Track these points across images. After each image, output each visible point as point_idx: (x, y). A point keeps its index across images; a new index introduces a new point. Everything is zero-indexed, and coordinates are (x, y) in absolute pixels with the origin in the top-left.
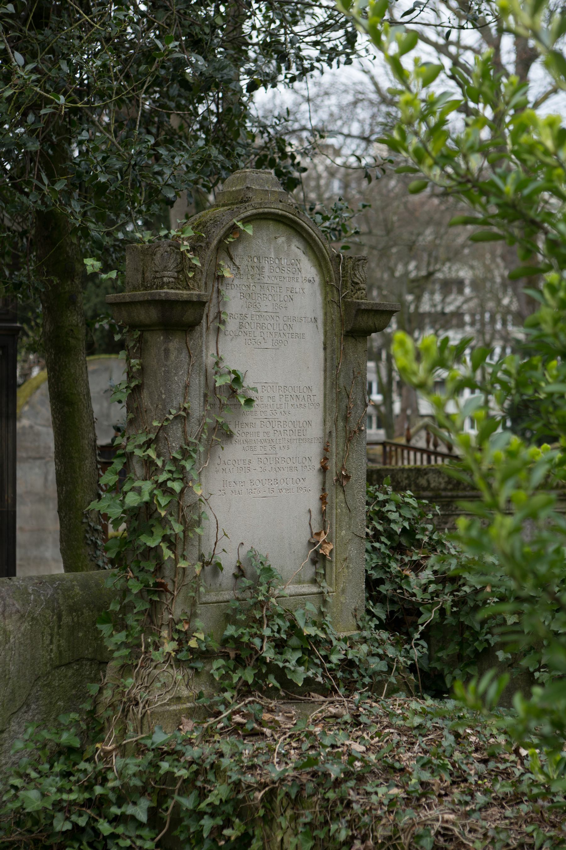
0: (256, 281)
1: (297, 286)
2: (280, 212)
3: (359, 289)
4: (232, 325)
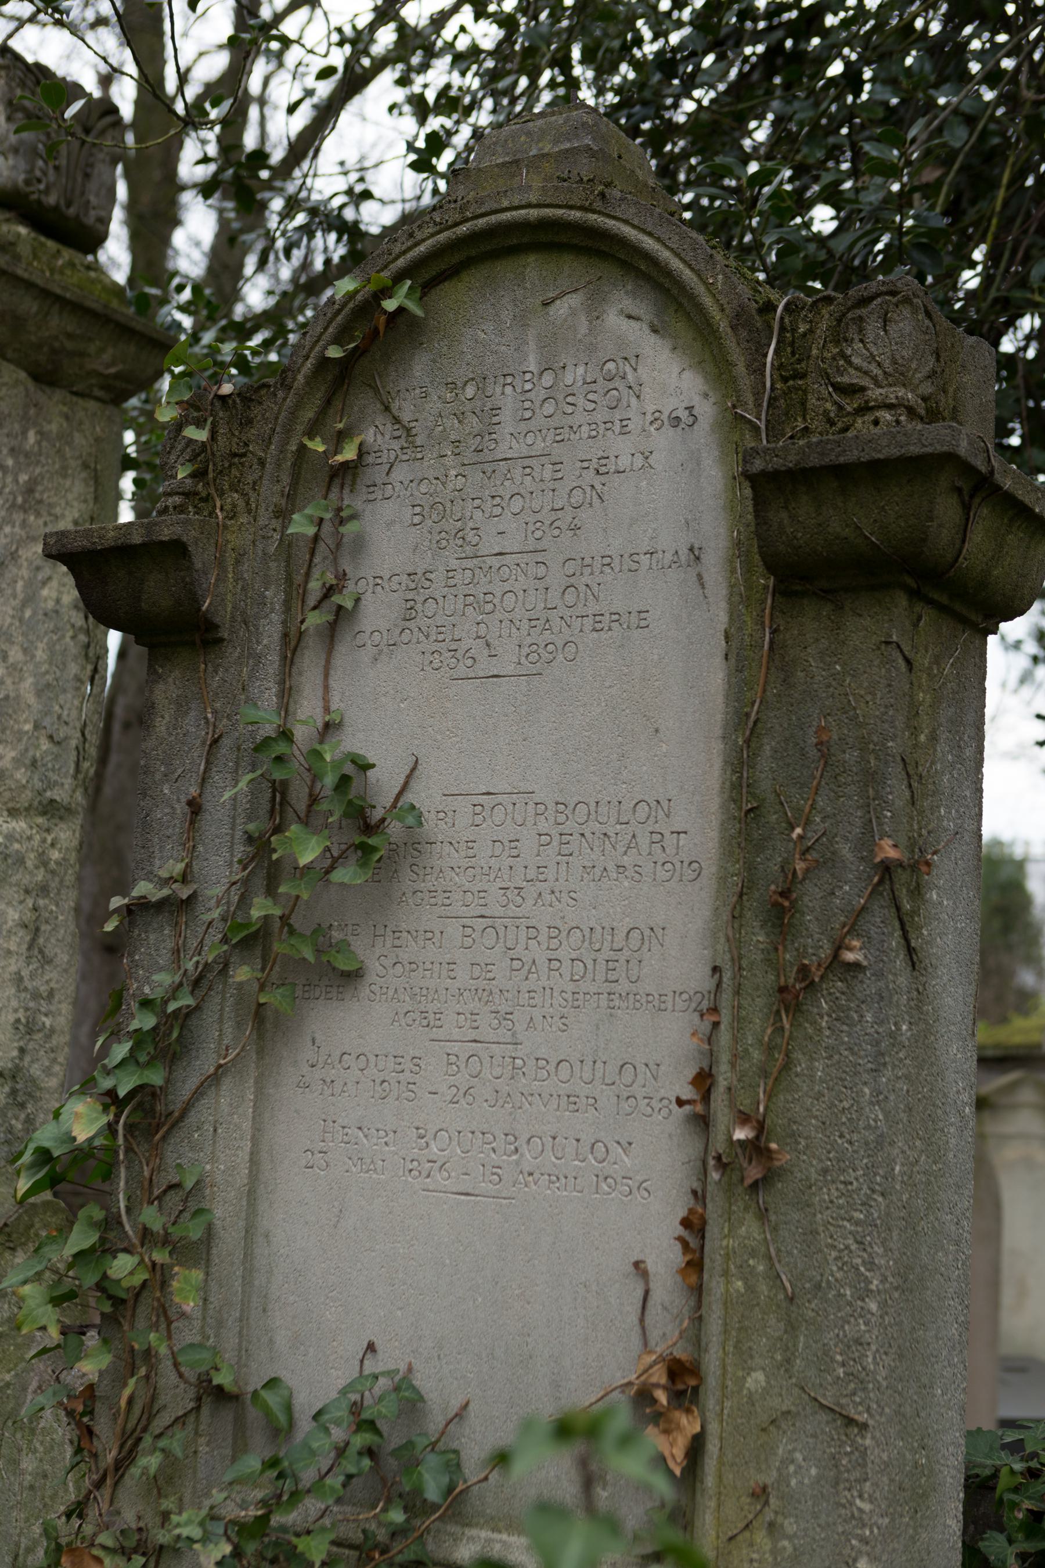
0: (469, 456)
1: (623, 450)
2: (534, 213)
3: (864, 409)
4: (377, 613)
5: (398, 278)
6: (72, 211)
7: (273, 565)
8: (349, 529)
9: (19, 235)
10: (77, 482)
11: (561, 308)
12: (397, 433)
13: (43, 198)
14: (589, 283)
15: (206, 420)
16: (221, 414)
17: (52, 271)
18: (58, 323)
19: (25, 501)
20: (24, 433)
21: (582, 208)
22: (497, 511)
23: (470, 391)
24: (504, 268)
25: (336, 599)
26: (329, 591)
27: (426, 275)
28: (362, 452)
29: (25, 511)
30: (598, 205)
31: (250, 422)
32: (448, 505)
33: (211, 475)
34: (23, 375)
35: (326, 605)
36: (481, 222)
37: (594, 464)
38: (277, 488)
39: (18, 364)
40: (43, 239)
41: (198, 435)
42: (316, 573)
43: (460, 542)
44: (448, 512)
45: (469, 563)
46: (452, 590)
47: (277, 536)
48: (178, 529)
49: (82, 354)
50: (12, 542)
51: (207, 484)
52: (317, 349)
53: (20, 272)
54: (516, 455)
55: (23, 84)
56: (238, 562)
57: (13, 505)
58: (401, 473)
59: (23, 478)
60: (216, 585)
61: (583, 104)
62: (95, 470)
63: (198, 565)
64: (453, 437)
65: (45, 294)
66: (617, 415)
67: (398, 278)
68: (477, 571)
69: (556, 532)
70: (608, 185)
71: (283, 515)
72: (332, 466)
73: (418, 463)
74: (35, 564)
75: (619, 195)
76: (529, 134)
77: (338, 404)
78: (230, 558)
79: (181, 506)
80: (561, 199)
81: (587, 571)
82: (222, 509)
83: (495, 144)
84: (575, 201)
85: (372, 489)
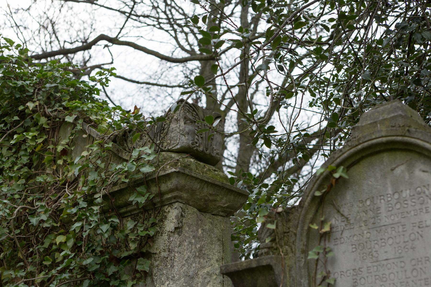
2: (384, 139)
5: (338, 166)
6: (208, 152)
7: (303, 270)
8: (329, 255)
9: (191, 161)
10: (216, 246)
11: (398, 171)
12: (343, 220)
13: (198, 148)
14: (407, 161)
15: (273, 222)
16: (279, 219)
17: (203, 173)
18: (207, 191)
19: (199, 255)
20: (197, 230)
21: (401, 136)
22: (383, 244)
23: (368, 203)
24: (375, 159)
25: (327, 281)
26: (324, 279)
27: (348, 164)
28: (331, 228)
29: (200, 258)
30: (407, 134)
31: (289, 220)
32: (365, 244)
33: (277, 240)
34: (196, 210)
35: (324, 283)
36: (366, 144)
37: (417, 224)
38: (302, 243)
39: (194, 206)
40: (199, 162)
41: (272, 227)
42: (319, 272)
43: (371, 257)
44: (365, 246)
45: (375, 264)
46: (370, 274)
47: (303, 260)
48: (269, 261)
49: (215, 201)
50: (196, 269)
51: (276, 244)
52: (311, 193)
53: (193, 175)
54: (388, 224)
55: (189, 111)
56: (290, 270)
57: (195, 256)
58: (346, 234)
59: (198, 246)
60: (283, 280)
61: (402, 103)
62: (222, 241)
63: (277, 273)
64: (364, 219)
65: (202, 181)
66: (424, 206)
67: (338, 166)
68: (379, 267)
69: (406, 250)
70: (409, 127)
71: (305, 252)
72: (320, 234)
73: (352, 230)
74: (204, 276)
75: (414, 130)
76: (378, 112)
77: (320, 211)
78: (287, 269)
79: (267, 252)
80: (394, 133)
81: (420, 263)
82: (282, 252)
83: (366, 117)
84: (399, 133)
85: (336, 240)
